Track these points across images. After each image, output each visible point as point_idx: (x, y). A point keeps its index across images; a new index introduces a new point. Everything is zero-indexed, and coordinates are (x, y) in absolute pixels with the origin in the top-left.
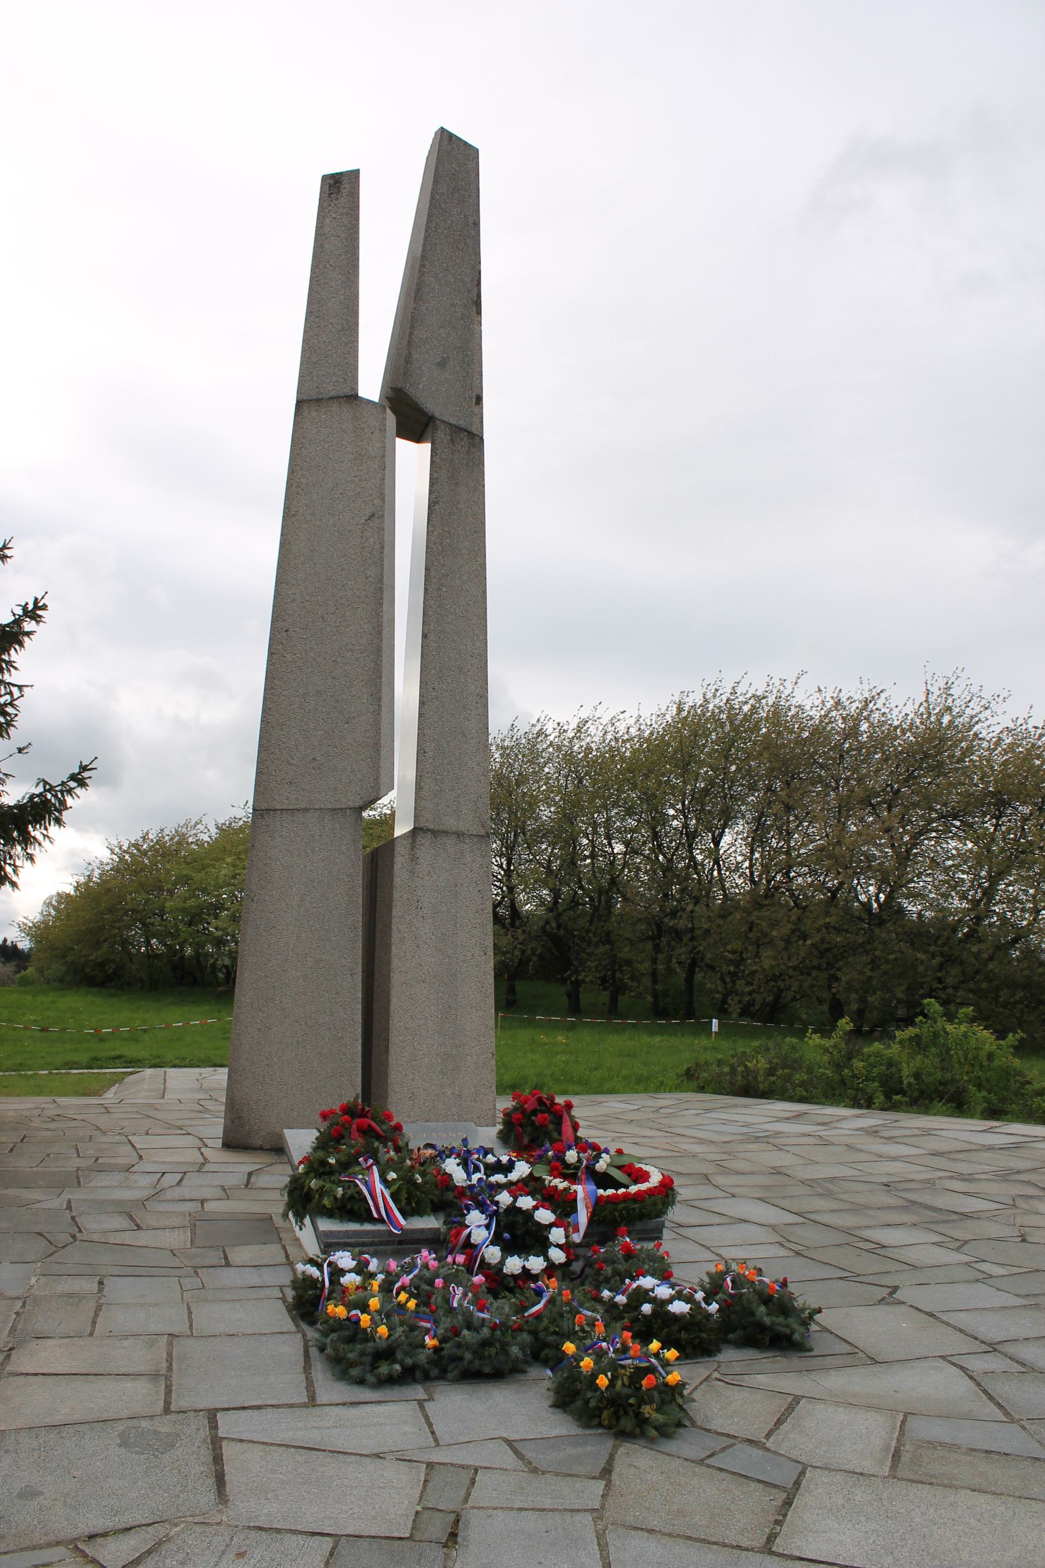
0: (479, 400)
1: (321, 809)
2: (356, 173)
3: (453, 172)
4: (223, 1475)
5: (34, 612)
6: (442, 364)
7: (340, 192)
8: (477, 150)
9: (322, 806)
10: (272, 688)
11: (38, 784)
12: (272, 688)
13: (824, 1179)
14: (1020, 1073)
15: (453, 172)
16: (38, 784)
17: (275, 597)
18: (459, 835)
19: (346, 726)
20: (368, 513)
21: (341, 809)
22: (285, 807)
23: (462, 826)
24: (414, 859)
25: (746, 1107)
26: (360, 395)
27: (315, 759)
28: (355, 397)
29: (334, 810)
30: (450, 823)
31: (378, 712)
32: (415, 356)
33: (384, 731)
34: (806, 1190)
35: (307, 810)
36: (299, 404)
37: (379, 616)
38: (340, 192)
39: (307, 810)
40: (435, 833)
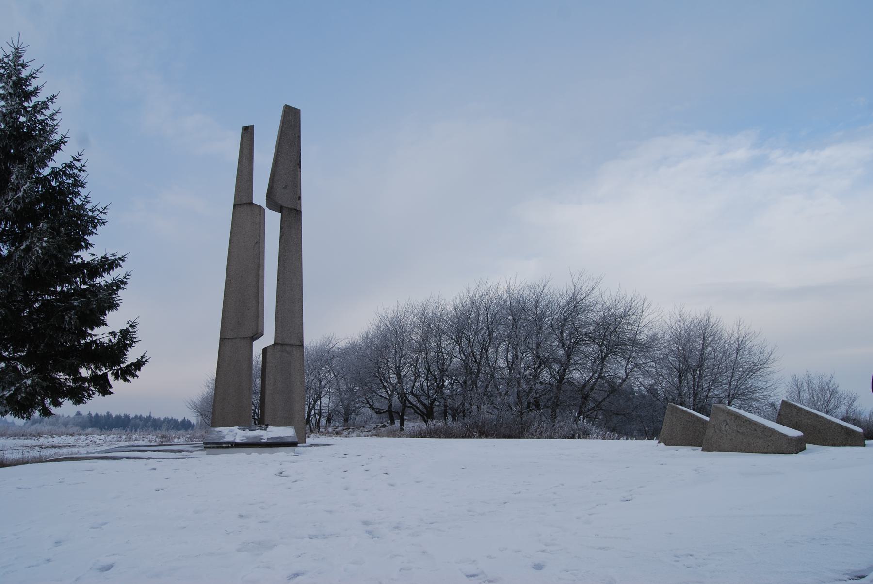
0: (300, 198)
2: (253, 126)
3: (291, 118)
4: (176, 421)
5: (122, 259)
6: (285, 188)
7: (248, 132)
11: (139, 364)
14: (36, 264)
15: (291, 118)
16: (139, 364)
23: (292, 342)
26: (254, 202)
28: (251, 203)
30: (287, 341)
31: (258, 306)
33: (260, 312)
36: (234, 205)
37: (258, 275)
38: (248, 132)
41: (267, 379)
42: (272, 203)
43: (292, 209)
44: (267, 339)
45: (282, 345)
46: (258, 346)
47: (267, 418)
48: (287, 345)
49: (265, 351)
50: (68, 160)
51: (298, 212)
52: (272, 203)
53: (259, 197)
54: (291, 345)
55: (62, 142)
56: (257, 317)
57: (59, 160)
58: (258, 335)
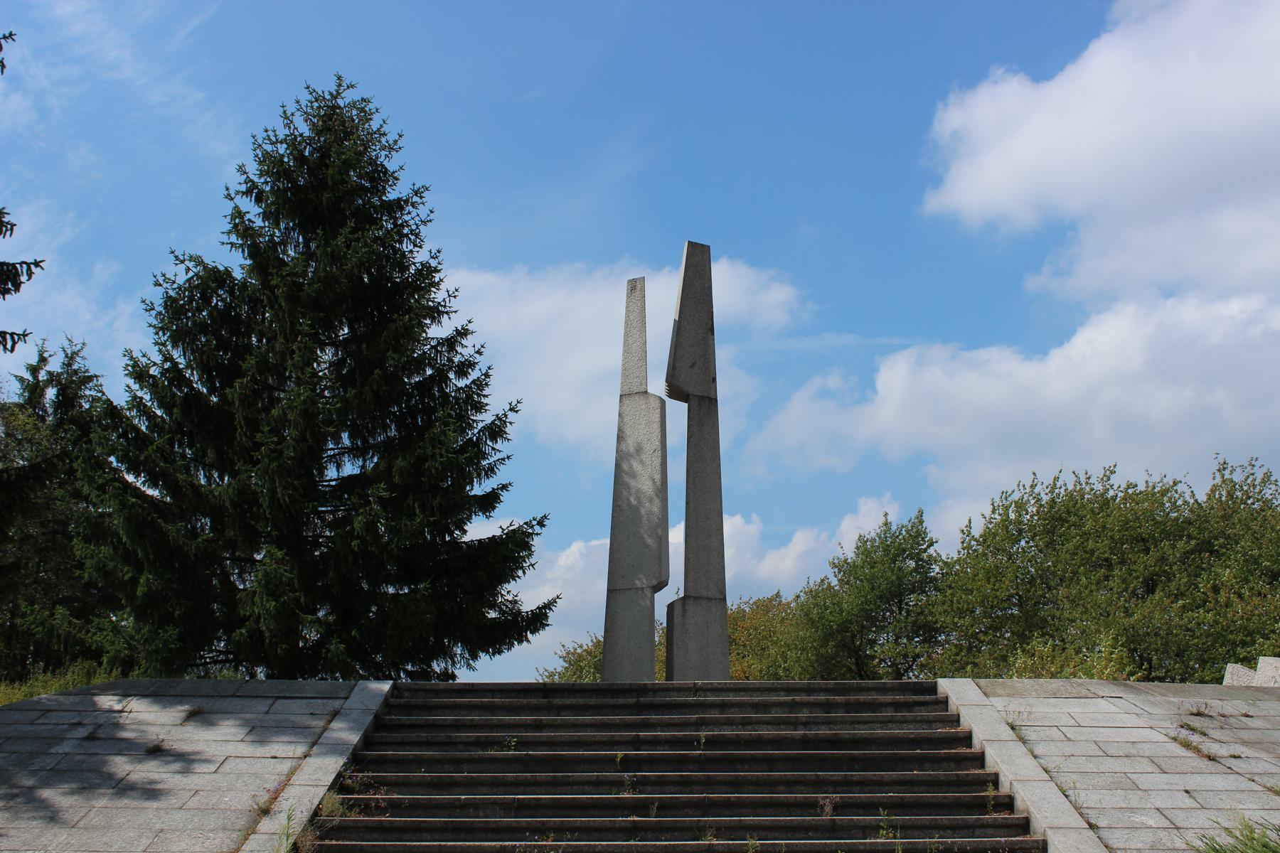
0: (714, 380)
5: (549, 605)
23: (710, 594)
28: (646, 392)
41: (675, 647)
42: (675, 392)
43: (704, 397)
44: (675, 588)
45: (695, 598)
46: (663, 599)
47: (642, 389)
48: (701, 598)
49: (671, 607)
50: (404, 195)
51: (713, 401)
52: (675, 392)
53: (657, 385)
54: (709, 599)
55: (538, 619)
56: (660, 558)
57: (438, 331)
58: (661, 585)
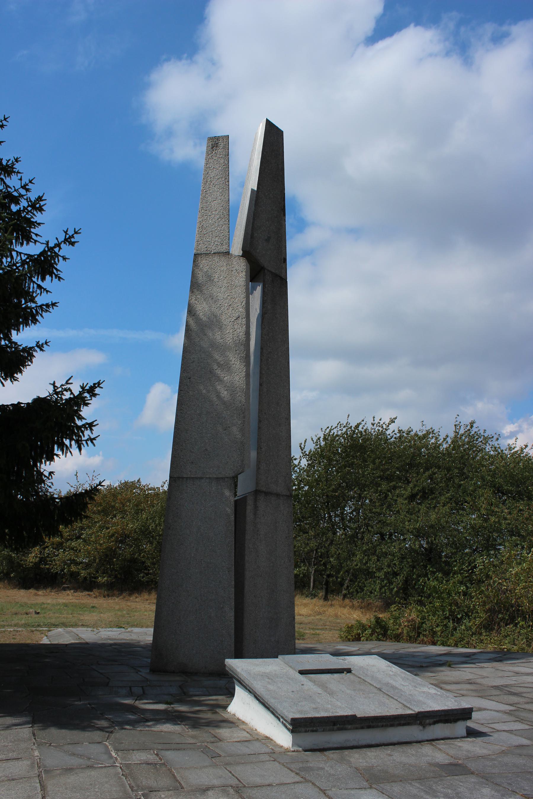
1: (210, 478)
6: (268, 240)
8: (283, 132)
9: (211, 476)
10: (181, 410)
12: (181, 410)
13: (502, 686)
17: (182, 359)
18: (278, 495)
19: (224, 432)
20: (37, 616)
21: (222, 478)
22: (189, 476)
24: (256, 507)
25: (415, 648)
27: (206, 450)
29: (217, 478)
32: (256, 235)
34: (498, 692)
35: (201, 478)
39: (201, 478)
40: (267, 494)
